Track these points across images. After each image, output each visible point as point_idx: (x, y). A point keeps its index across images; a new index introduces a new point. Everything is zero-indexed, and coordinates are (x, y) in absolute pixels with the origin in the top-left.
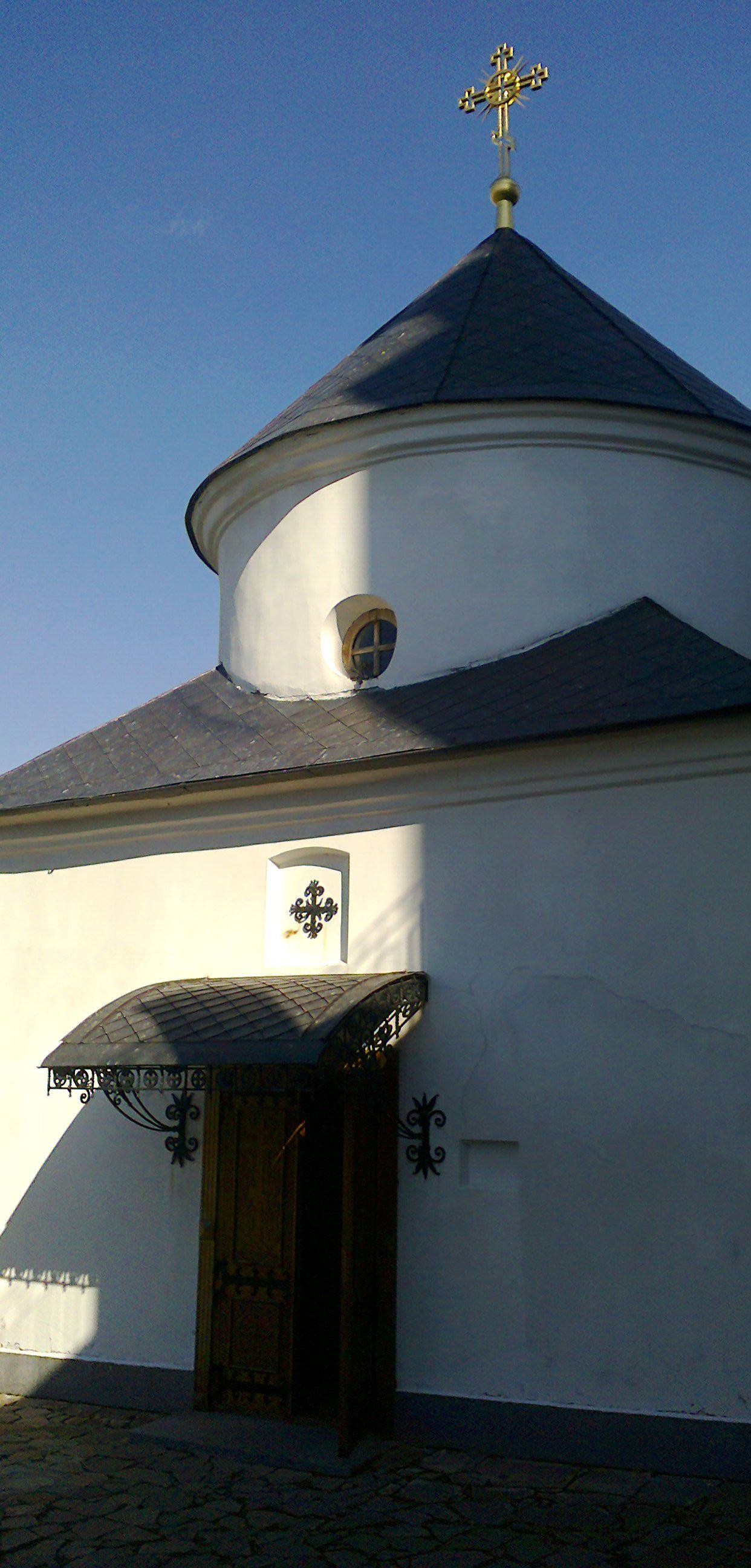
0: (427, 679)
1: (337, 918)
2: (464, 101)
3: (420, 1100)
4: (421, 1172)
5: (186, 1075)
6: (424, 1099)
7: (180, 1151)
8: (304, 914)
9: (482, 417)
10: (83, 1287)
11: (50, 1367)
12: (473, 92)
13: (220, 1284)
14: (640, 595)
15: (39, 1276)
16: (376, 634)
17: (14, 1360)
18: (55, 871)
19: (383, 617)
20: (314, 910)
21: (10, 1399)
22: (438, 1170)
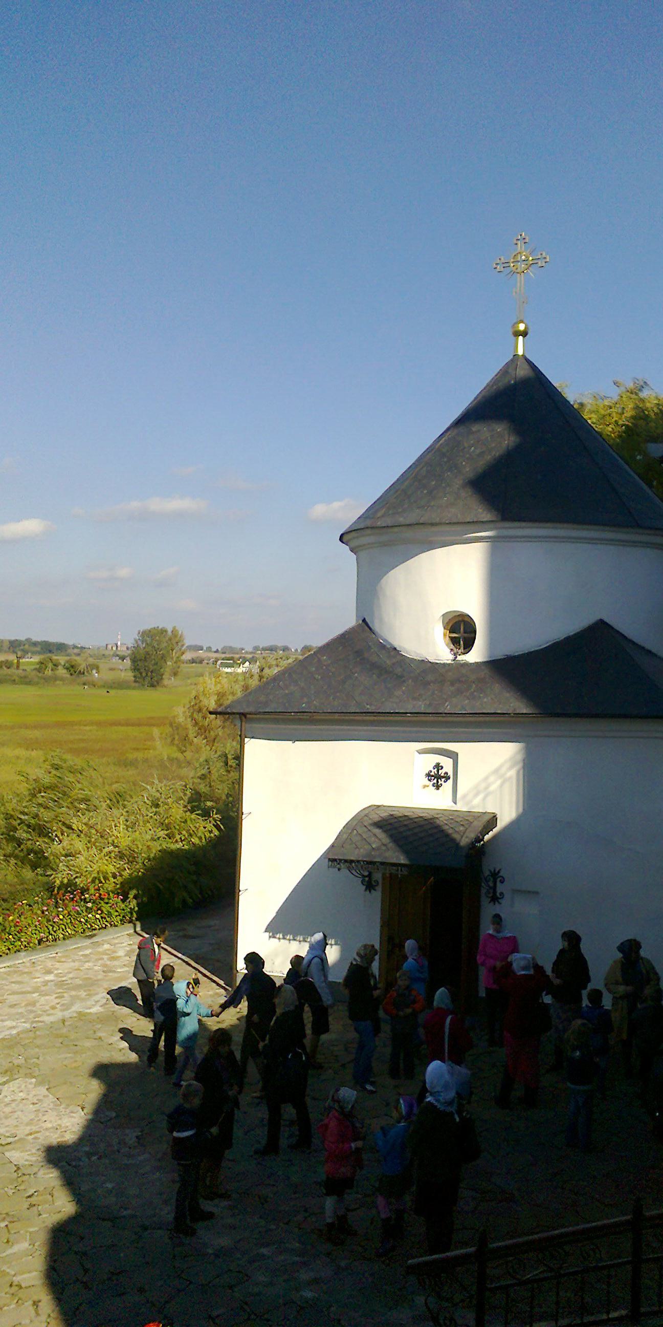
1: (450, 782)
3: (493, 871)
6: (495, 870)
8: (433, 778)
9: (523, 528)
14: (599, 618)
15: (275, 935)
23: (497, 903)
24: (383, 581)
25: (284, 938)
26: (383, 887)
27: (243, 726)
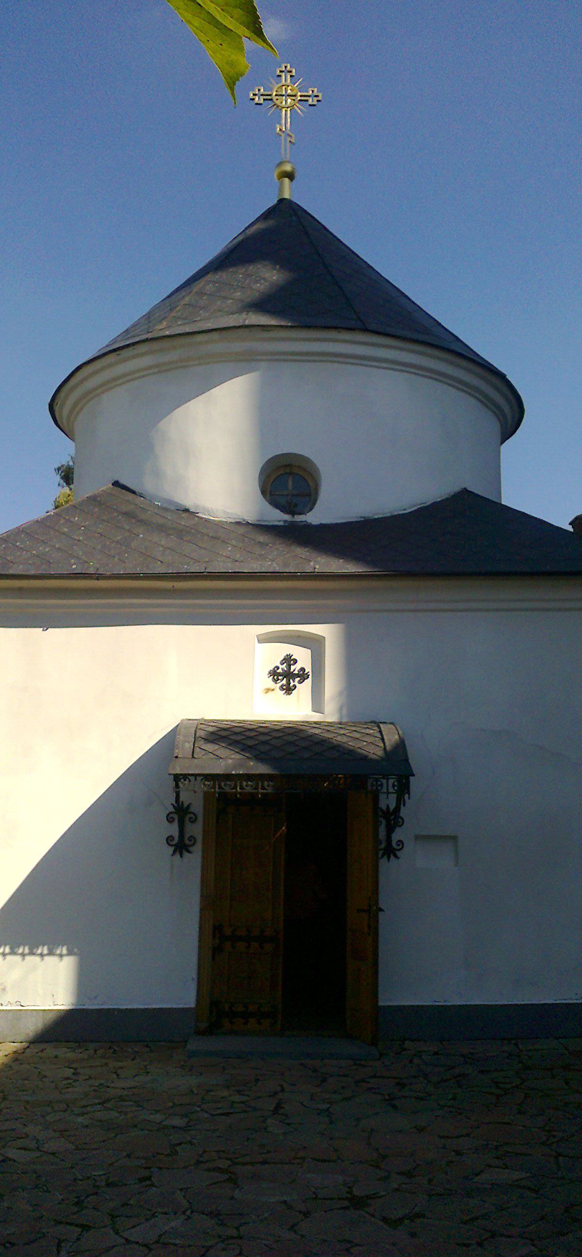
0: (344, 521)
1: (308, 682)
2: (254, 95)
4: (385, 857)
5: (387, 782)
7: (181, 846)
8: (280, 678)
10: (61, 956)
11: (50, 1017)
12: (262, 90)
14: (463, 487)
15: (35, 950)
17: (18, 1015)
18: (49, 629)
20: (289, 675)
21: (15, 1047)
23: (392, 857)
24: (163, 424)
25: (31, 953)
26: (204, 851)
27: (161, 334)
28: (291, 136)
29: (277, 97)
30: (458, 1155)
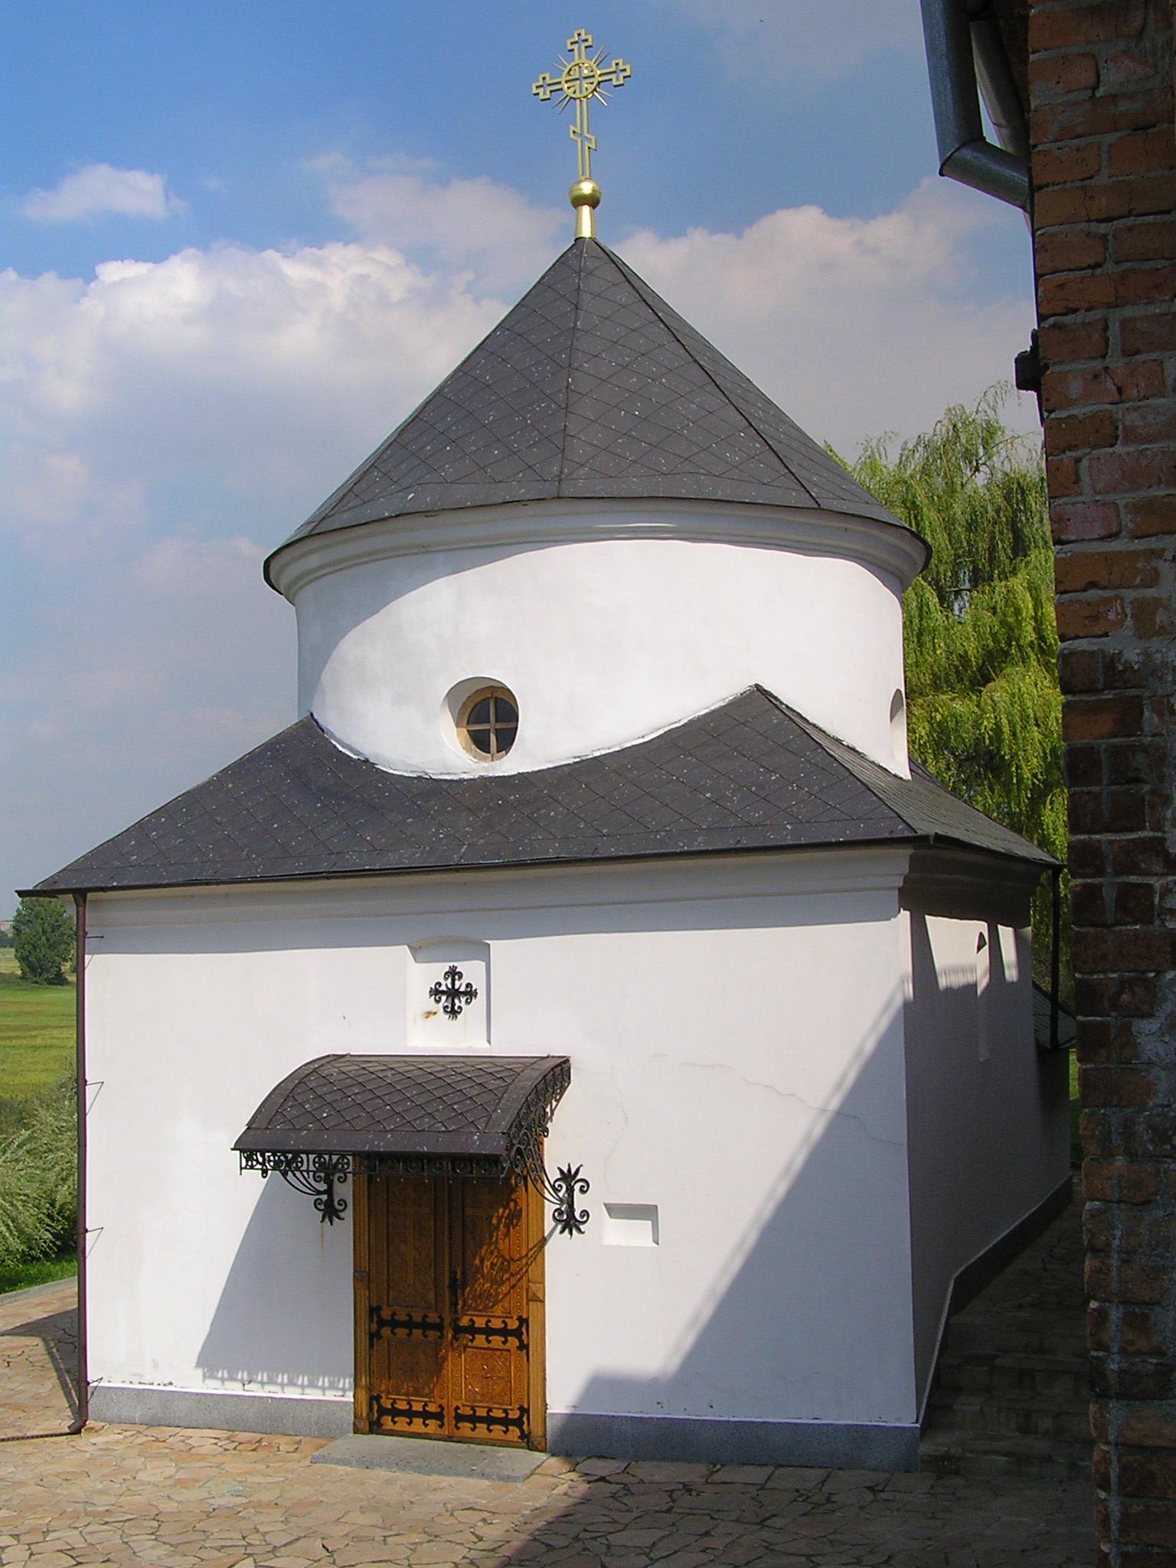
1: (479, 1001)
6: (569, 1170)
7: (330, 1211)
12: (548, 78)
13: (374, 1327)
16: (492, 711)
19: (499, 695)
22: (583, 1230)
28: (590, 140)
29: (569, 84)
30: (80, 1432)
